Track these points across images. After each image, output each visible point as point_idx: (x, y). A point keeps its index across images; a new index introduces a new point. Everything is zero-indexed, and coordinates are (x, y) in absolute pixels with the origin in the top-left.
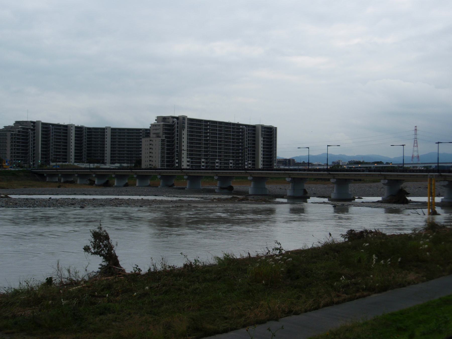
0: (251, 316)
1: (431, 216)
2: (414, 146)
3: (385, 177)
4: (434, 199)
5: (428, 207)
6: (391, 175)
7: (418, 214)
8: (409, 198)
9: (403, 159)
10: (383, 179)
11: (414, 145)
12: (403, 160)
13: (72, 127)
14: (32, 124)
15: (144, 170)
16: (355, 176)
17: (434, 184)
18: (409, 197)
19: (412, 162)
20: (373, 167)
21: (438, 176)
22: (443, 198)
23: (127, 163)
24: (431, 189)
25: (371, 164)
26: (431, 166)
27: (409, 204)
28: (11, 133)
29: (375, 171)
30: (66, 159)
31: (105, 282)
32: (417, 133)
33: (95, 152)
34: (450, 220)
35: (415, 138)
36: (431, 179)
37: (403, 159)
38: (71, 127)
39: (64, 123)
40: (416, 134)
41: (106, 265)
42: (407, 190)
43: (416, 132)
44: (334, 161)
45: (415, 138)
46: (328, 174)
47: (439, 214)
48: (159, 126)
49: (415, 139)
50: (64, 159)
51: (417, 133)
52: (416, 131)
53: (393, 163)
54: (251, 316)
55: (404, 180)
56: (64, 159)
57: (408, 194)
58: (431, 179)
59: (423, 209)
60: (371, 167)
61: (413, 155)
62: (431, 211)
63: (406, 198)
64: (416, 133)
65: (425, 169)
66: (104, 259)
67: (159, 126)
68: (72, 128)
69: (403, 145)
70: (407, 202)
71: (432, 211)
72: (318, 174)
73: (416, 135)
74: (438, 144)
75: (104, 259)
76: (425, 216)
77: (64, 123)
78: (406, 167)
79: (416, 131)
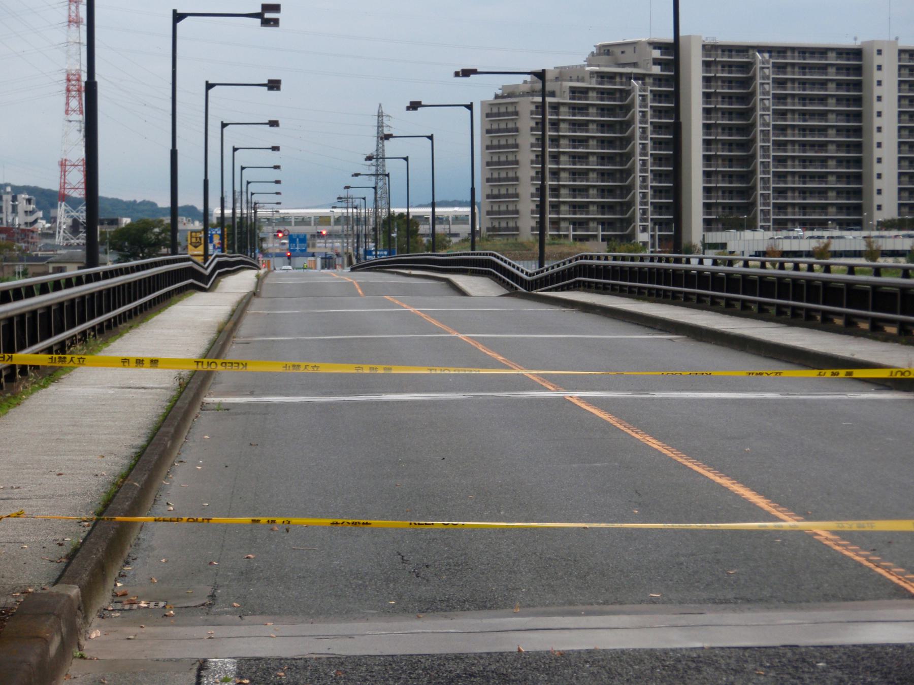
0: (673, 662)
10: (872, 237)
13: (879, 52)
14: (657, 54)
23: (807, 225)
28: (533, 103)
30: (858, 209)
31: (9, 602)
33: (823, 186)
38: (875, 52)
39: (855, 39)
41: (607, 683)
48: (242, 167)
50: (848, 209)
54: (673, 662)
56: (848, 209)
67: (242, 167)
68: (877, 60)
74: (469, 199)
77: (855, 39)
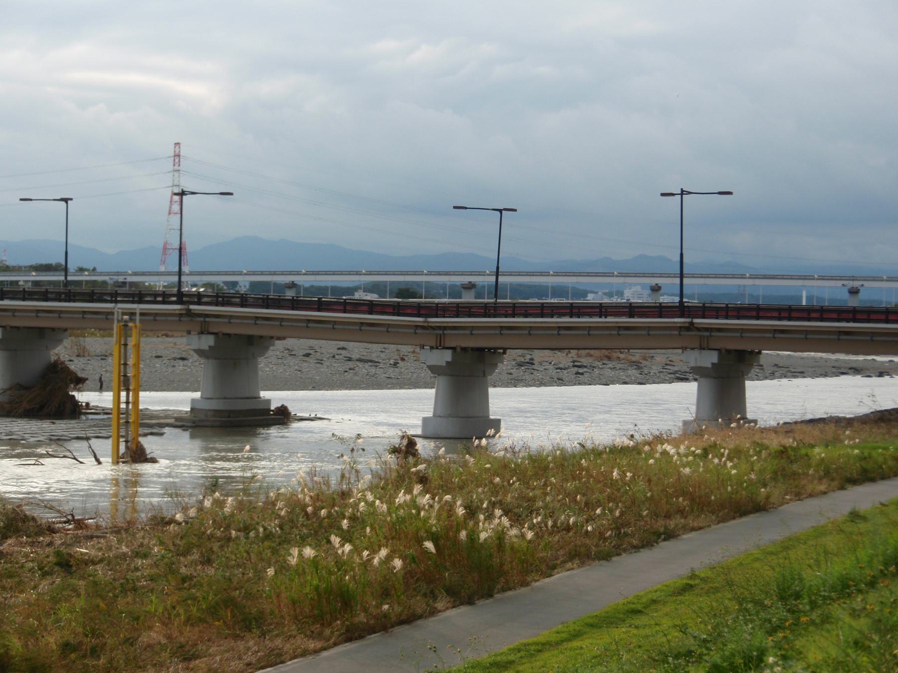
1: (124, 468)
2: (170, 213)
3: (204, 325)
4: (136, 402)
5: (113, 431)
6: (14, 311)
7: (75, 458)
8: (82, 397)
9: (66, 253)
11: (170, 207)
12: (64, 253)
15: (534, 317)
16: (37, 316)
17: (137, 346)
18: (84, 393)
19: (162, 269)
20: (24, 281)
21: (181, 315)
22: (197, 395)
24: (125, 364)
25: (360, 288)
26: (235, 284)
27: (83, 417)
29: (25, 295)
32: (179, 166)
34: (897, 449)
35: (173, 186)
36: (125, 329)
37: (66, 253)
40: (179, 170)
42: (76, 366)
43: (177, 165)
44: (32, 264)
45: (173, 186)
46: (184, 312)
47: (154, 461)
49: (175, 188)
51: (181, 168)
52: (177, 160)
53: (98, 270)
55: (66, 330)
57: (79, 382)
58: (125, 329)
59: (93, 442)
60: (17, 282)
61: (166, 244)
62: (122, 448)
63: (73, 396)
64: (176, 167)
65: (210, 292)
66: (407, 495)
69: (66, 200)
70: (74, 411)
71: (127, 447)
72: (38, 311)
73: (176, 174)
75: (407, 495)
76: (100, 466)
78: (147, 284)
79: (177, 160)
